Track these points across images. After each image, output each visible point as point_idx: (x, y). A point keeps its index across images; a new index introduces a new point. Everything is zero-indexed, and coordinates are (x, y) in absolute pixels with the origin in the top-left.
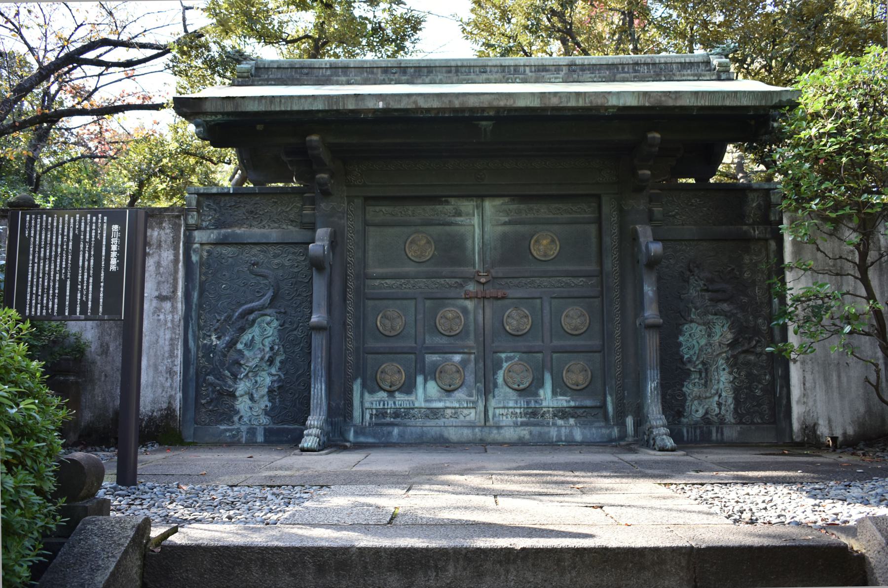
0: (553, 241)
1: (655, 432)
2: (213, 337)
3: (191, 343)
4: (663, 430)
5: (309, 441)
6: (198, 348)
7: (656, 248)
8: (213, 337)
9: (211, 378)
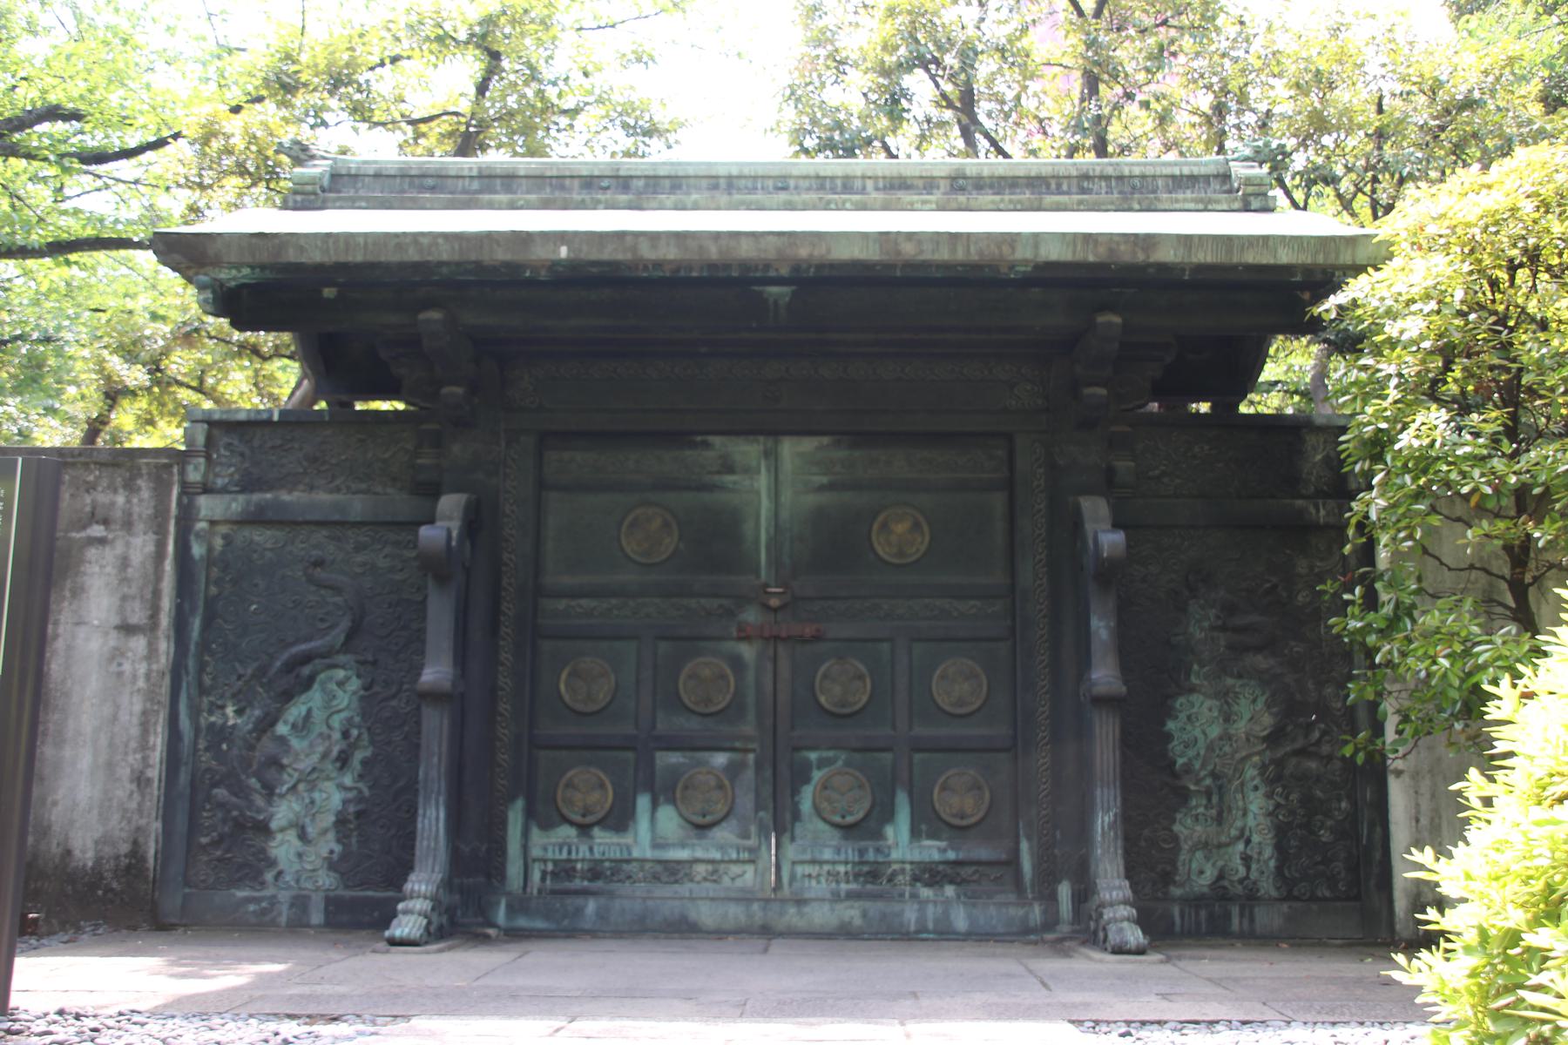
0: (916, 526)
1: (1108, 914)
2: (230, 710)
3: (185, 723)
4: (1125, 911)
5: (406, 926)
6: (197, 730)
7: (1111, 541)
8: (230, 710)
9: (221, 793)
